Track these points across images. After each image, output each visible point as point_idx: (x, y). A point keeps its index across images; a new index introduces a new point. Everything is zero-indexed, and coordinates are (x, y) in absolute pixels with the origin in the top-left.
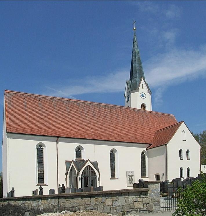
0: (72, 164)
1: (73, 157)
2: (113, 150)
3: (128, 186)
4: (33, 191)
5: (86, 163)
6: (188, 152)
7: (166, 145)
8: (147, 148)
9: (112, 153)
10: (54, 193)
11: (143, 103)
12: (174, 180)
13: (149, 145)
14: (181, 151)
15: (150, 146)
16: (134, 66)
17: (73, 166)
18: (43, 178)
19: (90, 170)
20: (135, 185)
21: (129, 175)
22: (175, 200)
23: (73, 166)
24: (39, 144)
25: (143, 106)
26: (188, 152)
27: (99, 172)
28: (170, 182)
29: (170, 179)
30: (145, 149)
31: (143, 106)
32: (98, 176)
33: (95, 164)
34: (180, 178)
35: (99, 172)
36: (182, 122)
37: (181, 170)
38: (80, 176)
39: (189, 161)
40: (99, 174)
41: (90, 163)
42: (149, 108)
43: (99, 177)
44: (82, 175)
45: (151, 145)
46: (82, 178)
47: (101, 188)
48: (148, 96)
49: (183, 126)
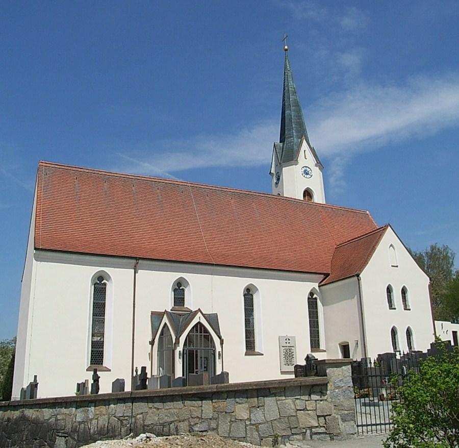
0: (165, 320)
3: (282, 373)
7: (358, 276)
8: (320, 283)
9: (249, 295)
12: (381, 358)
13: (323, 276)
17: (166, 324)
22: (386, 408)
23: (166, 324)
24: (98, 275)
25: (308, 193)
27: (220, 337)
28: (372, 362)
29: (373, 356)
31: (308, 193)
33: (213, 319)
35: (220, 337)
36: (386, 226)
38: (180, 348)
40: (222, 343)
43: (221, 350)
44: (185, 344)
45: (327, 275)
46: (185, 352)
47: (225, 376)
48: (316, 172)
49: (389, 236)
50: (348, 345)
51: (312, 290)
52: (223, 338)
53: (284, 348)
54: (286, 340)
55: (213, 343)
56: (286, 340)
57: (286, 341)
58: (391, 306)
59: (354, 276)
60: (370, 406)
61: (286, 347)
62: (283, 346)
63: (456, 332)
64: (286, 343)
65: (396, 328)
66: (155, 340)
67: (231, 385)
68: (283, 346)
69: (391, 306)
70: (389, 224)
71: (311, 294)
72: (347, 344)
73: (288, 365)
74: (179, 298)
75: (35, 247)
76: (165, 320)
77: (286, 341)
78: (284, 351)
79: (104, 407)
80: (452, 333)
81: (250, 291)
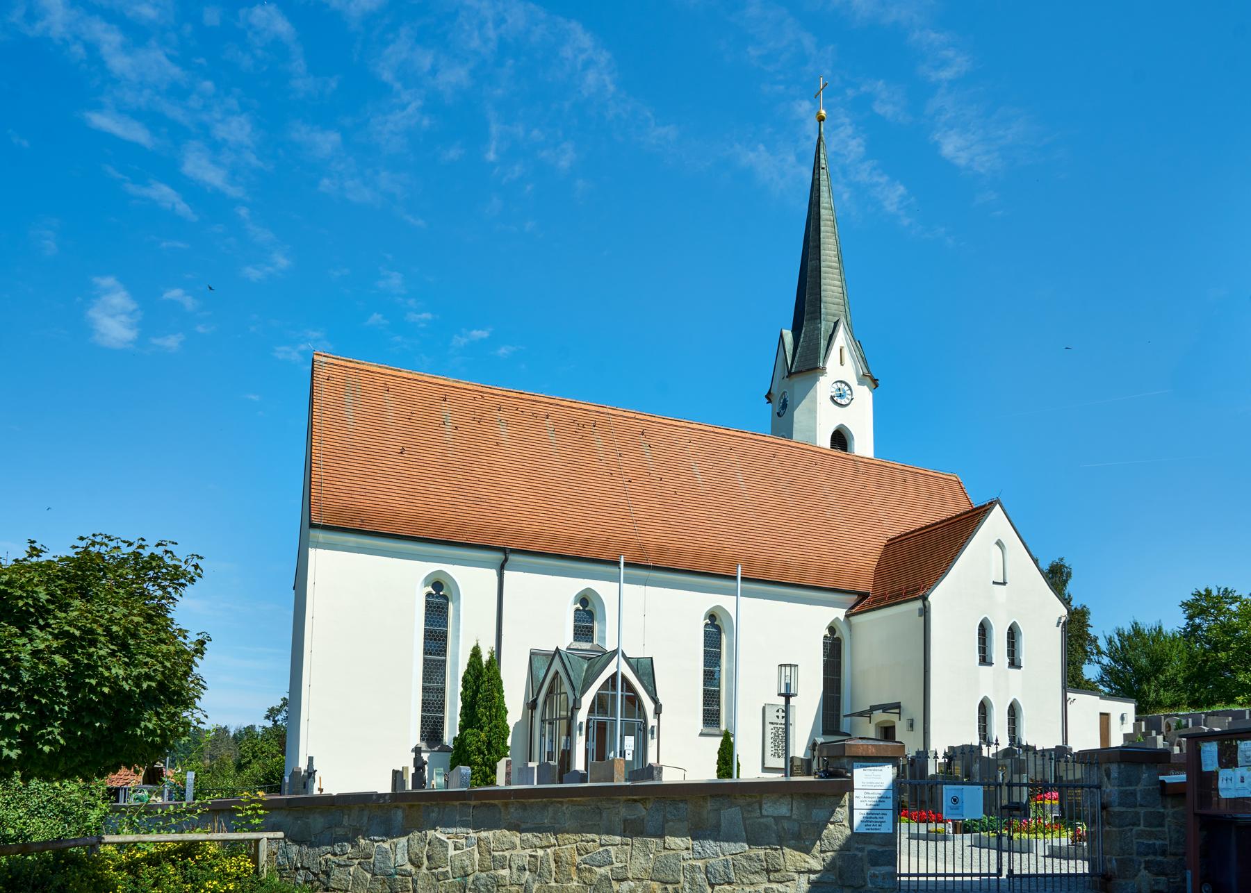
0: (557, 665)
1: (564, 638)
2: (718, 612)
3: (765, 769)
4: (395, 773)
5: (638, 678)
6: (1013, 633)
7: (925, 598)
8: (852, 608)
9: (715, 629)
10: (661, 780)
11: (842, 425)
12: (953, 754)
13: (856, 597)
14: (984, 630)
15: (863, 602)
16: (812, 271)
17: (557, 673)
18: (423, 711)
19: (1081, 808)
20: (791, 765)
21: (776, 720)
22: (958, 843)
23: (557, 673)
24: (434, 579)
25: (840, 439)
26: (1013, 633)
27: (655, 700)
28: (941, 755)
29: (940, 744)
30: (841, 613)
31: (840, 439)
32: (652, 721)
33: (645, 669)
34: (976, 742)
35: (655, 700)
36: (991, 505)
37: (984, 709)
38: (582, 716)
39: (1056, 625)
40: (658, 711)
41: (623, 662)
42: (863, 445)
43: (656, 724)
44: (591, 711)
45: (863, 596)
46: (591, 724)
47: (655, 772)
48: (864, 396)
49: (995, 524)
50: (894, 727)
51: (833, 622)
52: (661, 701)
53: (772, 726)
54: (778, 711)
55: (642, 712)
56: (778, 711)
57: (778, 714)
58: (985, 660)
59: (916, 599)
60: (936, 841)
61: (777, 724)
62: (771, 723)
63: (775, 432)
64: (778, 717)
65: (988, 698)
66: (872, 845)
67: (664, 783)
68: (771, 723)
69: (985, 660)
70: (999, 500)
71: (832, 629)
72: (891, 725)
73: (779, 757)
74: (584, 630)
75: (310, 521)
76: (557, 665)
77: (778, 714)
78: (773, 731)
79: (518, 835)
80: (1098, 717)
81: (715, 620)
